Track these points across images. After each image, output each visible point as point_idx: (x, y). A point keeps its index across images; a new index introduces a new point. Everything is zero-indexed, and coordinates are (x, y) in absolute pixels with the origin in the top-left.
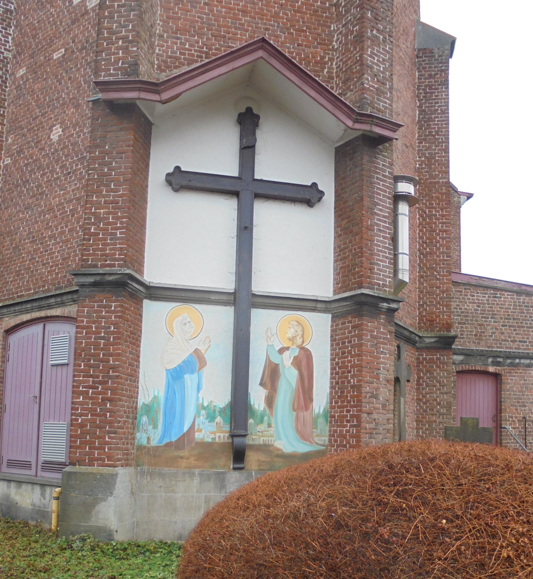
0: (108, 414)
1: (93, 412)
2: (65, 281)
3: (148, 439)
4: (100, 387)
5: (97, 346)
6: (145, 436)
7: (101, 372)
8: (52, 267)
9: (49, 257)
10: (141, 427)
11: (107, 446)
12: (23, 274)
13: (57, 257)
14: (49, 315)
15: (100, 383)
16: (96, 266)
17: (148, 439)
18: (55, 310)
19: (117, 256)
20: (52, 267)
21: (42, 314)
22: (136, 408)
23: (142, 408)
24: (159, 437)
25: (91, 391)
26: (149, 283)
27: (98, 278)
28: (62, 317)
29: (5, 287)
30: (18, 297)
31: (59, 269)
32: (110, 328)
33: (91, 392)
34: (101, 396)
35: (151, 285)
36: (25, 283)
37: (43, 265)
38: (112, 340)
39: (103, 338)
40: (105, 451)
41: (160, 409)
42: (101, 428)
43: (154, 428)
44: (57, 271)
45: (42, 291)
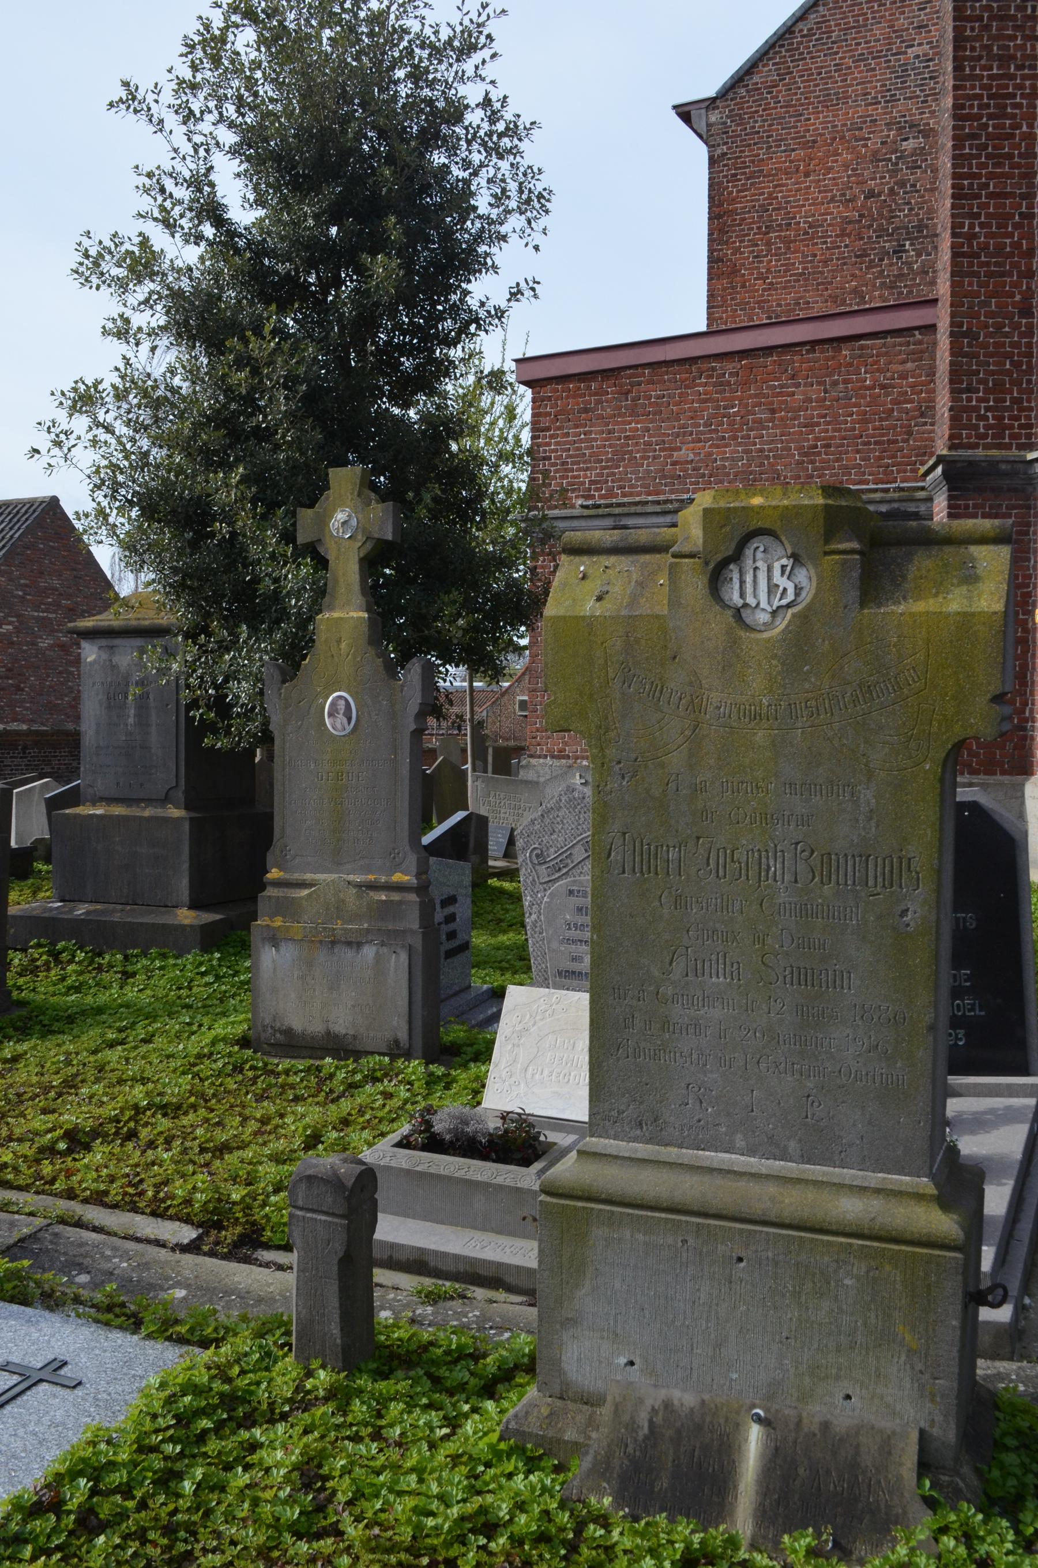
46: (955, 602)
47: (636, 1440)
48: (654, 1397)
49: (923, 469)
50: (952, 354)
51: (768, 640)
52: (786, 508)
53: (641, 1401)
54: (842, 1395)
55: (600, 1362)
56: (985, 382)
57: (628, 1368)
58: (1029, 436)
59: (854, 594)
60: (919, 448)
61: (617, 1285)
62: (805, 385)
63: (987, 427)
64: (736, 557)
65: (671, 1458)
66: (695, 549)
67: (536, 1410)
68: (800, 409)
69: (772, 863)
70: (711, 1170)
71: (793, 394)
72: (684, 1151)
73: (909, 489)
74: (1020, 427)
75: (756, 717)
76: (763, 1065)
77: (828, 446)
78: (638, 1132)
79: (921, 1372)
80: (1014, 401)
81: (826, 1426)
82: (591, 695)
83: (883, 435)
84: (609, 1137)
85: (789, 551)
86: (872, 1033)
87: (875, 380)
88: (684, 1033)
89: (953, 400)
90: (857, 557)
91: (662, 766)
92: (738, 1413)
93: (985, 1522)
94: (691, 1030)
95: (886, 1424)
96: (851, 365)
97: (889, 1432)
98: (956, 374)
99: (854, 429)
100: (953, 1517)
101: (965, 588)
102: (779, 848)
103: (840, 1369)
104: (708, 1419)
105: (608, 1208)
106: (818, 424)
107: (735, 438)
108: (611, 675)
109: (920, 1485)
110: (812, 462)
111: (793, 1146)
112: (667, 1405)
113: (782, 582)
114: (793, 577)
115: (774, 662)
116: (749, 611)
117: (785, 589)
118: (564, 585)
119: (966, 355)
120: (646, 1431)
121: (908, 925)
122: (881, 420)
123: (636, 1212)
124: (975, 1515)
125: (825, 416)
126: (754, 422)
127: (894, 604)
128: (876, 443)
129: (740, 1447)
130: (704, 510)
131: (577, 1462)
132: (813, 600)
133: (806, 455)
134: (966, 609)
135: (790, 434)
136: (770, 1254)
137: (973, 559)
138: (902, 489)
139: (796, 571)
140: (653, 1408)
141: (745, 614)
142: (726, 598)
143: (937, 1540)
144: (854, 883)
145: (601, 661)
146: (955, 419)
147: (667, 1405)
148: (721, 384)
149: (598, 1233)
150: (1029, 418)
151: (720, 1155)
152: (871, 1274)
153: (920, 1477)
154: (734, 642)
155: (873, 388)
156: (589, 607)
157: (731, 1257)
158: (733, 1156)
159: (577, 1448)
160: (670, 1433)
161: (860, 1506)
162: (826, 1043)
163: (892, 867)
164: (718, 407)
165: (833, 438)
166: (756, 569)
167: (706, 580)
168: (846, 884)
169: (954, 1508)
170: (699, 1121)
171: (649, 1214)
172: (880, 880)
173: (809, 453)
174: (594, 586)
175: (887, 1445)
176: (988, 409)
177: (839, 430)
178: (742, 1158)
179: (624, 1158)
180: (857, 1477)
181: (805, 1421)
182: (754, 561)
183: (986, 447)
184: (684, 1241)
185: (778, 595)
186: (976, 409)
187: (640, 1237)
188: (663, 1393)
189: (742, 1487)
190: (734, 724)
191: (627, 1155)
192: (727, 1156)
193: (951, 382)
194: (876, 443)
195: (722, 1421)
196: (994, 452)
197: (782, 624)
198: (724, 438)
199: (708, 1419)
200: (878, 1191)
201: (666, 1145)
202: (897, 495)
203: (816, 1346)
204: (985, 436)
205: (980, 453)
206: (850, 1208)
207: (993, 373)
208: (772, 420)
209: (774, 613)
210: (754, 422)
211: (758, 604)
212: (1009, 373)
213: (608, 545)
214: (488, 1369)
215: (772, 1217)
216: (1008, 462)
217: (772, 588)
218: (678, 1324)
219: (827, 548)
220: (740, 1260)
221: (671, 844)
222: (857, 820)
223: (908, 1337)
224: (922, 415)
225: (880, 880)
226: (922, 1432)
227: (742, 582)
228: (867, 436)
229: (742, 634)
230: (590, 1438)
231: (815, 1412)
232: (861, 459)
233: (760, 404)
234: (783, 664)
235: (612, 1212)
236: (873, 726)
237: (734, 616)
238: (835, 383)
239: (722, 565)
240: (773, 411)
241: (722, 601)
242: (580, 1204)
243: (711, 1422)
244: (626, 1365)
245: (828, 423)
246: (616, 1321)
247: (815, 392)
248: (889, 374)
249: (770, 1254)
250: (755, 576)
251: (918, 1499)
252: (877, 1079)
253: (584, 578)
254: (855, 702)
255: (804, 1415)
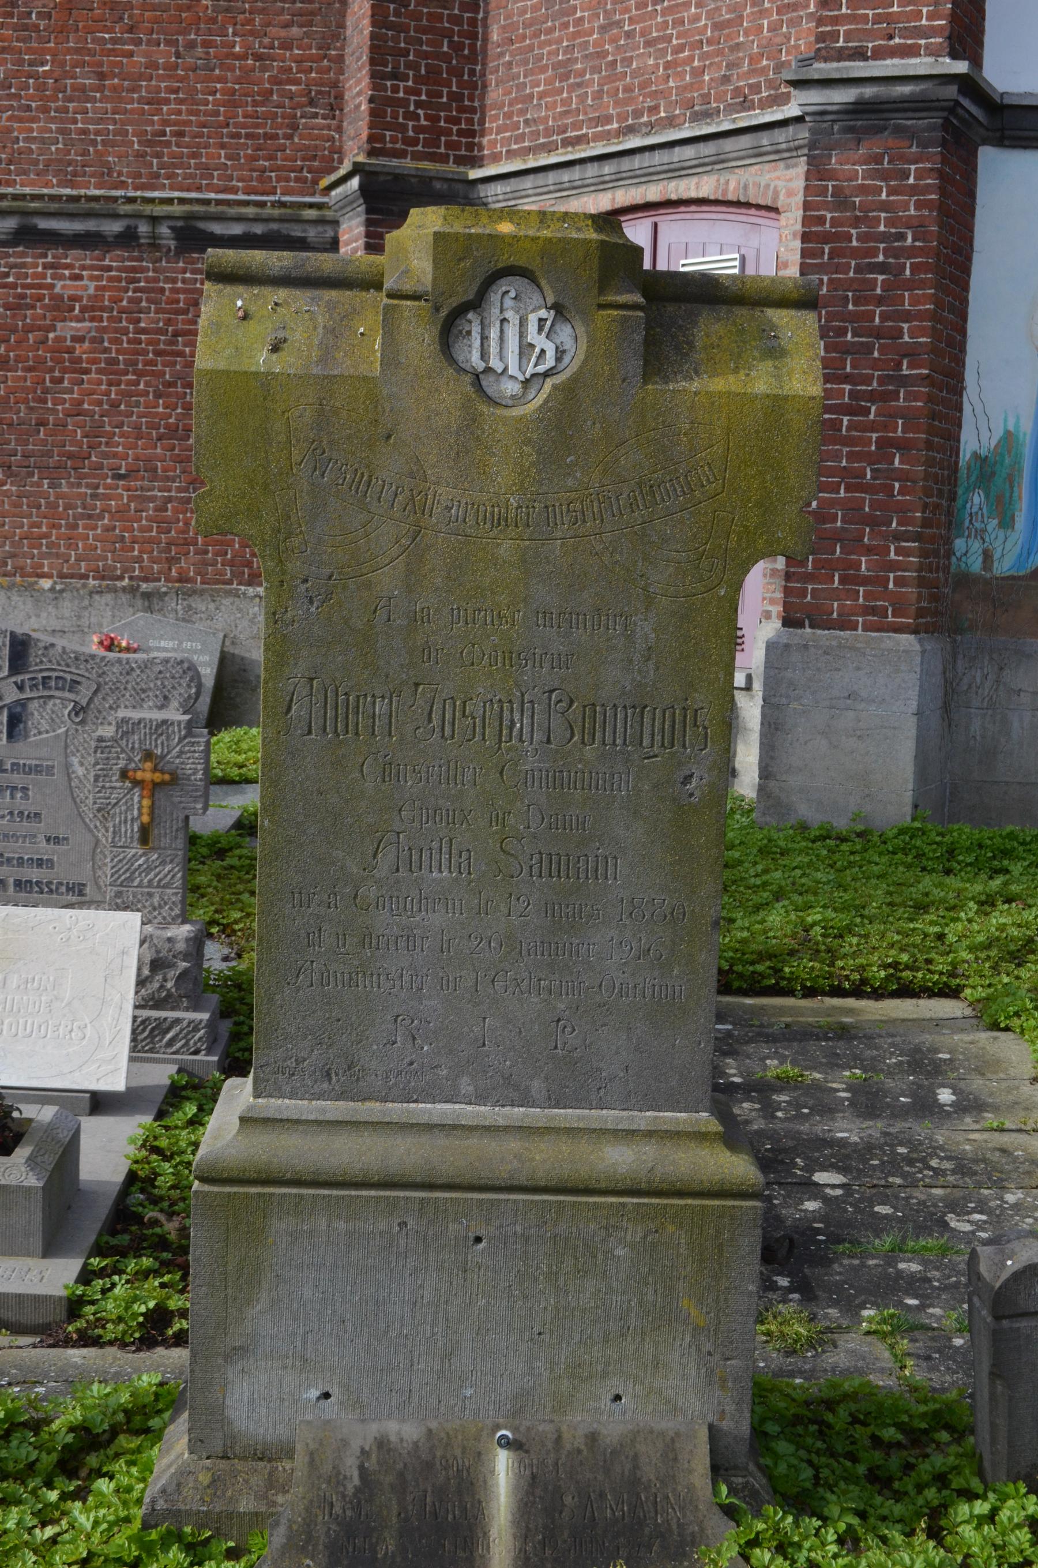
0: (897, 485)
1: (854, 482)
2: (726, 92)
3: (987, 556)
4: (873, 409)
5: (863, 292)
6: (976, 546)
7: (875, 365)
8: (680, 49)
9: (670, 19)
10: (967, 523)
11: (892, 575)
12: (582, 73)
13: (697, 18)
14: (674, 197)
15: (873, 397)
16: (859, 54)
17: (987, 556)
18: (694, 180)
19: (924, 22)
20: (680, 49)
21: (653, 193)
22: (955, 468)
23: (968, 469)
24: (1017, 549)
25: (846, 420)
26: (1002, 94)
27: (869, 91)
28: (716, 202)
29: (523, 112)
30: (568, 143)
31: (703, 57)
32: (902, 237)
33: (845, 423)
34: (874, 435)
35: (1007, 101)
36: (589, 102)
37: (648, 44)
38: (908, 272)
39: (882, 268)
40: (886, 587)
41: (1020, 471)
42: (872, 522)
43: (1002, 525)
44: (696, 63)
45: (645, 124)
46: (761, 381)
47: (344, 1496)
48: (362, 1435)
49: (325, 182)
50: (374, 23)
51: (521, 418)
52: (549, 240)
53: (345, 1443)
54: (610, 1396)
55: (282, 1400)
56: (414, 66)
57: (322, 1402)
58: (470, 147)
59: (635, 365)
60: (307, 148)
61: (308, 1293)
62: (149, 42)
63: (418, 129)
64: (477, 303)
65: (395, 1512)
66: (420, 289)
67: (191, 1478)
68: (141, 77)
69: (517, 717)
70: (429, 1127)
71: (130, 54)
72: (390, 1105)
73: (293, 205)
74: (461, 133)
75: (500, 522)
76: (499, 985)
77: (180, 134)
78: (325, 1085)
79: (710, 1354)
80: (454, 97)
81: (593, 1438)
82: (266, 486)
83: (257, 126)
84: (282, 1096)
85: (551, 300)
86: (643, 935)
87: (248, 47)
88: (392, 947)
89: (375, 87)
90: (641, 314)
91: (368, 585)
92: (478, 1439)
93: (796, 1523)
94: (402, 944)
95: (667, 1425)
96: (213, 20)
97: (671, 1433)
98: (378, 53)
99: (217, 113)
100: (761, 1526)
101: (770, 363)
102: (526, 698)
103: (607, 1364)
104: (439, 1454)
105: (294, 1191)
106: (167, 101)
107: (46, 110)
108: (296, 457)
109: (716, 1493)
110: (159, 155)
111: (537, 1086)
112: (382, 1443)
113: (540, 341)
114: (554, 336)
115: (527, 449)
116: (492, 378)
117: (543, 351)
118: (217, 326)
119: (391, 26)
120: (356, 1481)
121: (691, 795)
122: (255, 103)
123: (335, 1192)
124: (783, 1519)
125: (176, 91)
126: (74, 89)
127: (685, 379)
128: (248, 136)
129: (485, 1482)
130: (435, 234)
131: (258, 1540)
132: (581, 368)
133: (149, 143)
134: (775, 391)
135: (125, 112)
136: (519, 1229)
137: (774, 327)
138: (283, 205)
139: (557, 327)
140: (363, 1451)
141: (486, 381)
142: (461, 359)
143: (746, 1558)
144: (625, 743)
145: (282, 438)
146: (376, 115)
147: (382, 1443)
148: (25, 28)
149: (280, 1226)
150: (470, 121)
151: (438, 1106)
152: (649, 1239)
153: (715, 1483)
154: (473, 420)
155: (243, 57)
156: (261, 360)
157: (466, 1237)
158: (457, 1106)
159: (257, 1520)
160: (389, 1479)
161: (647, 1531)
162: (583, 951)
163: (674, 722)
164: (20, 62)
165: (189, 123)
166: (504, 321)
167: (435, 331)
168: (614, 743)
169: (758, 1514)
170: (411, 1063)
171: (353, 1193)
172: (658, 738)
173: (154, 141)
174: (261, 331)
175: (671, 1450)
176: (419, 104)
177: (197, 113)
178: (469, 1108)
179: (307, 1122)
180: (639, 1497)
181: (566, 1436)
182: (502, 311)
183: (417, 157)
184: (403, 1224)
185: (533, 359)
186: (405, 103)
187: (341, 1225)
188: (374, 1429)
189: (494, 1533)
190: (469, 531)
191: (312, 1117)
192: (449, 1106)
193: (373, 62)
194: (248, 136)
195: (458, 1452)
196: (425, 165)
197: (538, 398)
198: (29, 108)
199: (439, 1454)
200: (650, 1134)
201: (365, 1100)
202: (276, 212)
203: (577, 1339)
204: (415, 142)
205: (408, 164)
206: (620, 1159)
207: (426, 55)
208: (101, 89)
209: (526, 383)
210: (74, 89)
211: (506, 369)
212: (446, 58)
213: (276, 272)
214: (59, 1438)
215: (541, 1178)
216: (446, 180)
217: (525, 348)
218: (392, 1334)
219: (603, 299)
220: (478, 1240)
221: (378, 693)
222: (631, 661)
223: (694, 1312)
224: (311, 103)
225: (658, 738)
226: (711, 1427)
227: (484, 338)
228: (237, 125)
229: (485, 409)
230: (274, 1504)
231: (577, 1423)
232: (227, 158)
233: (82, 64)
234: (539, 452)
235: (301, 1197)
236: (655, 538)
237: (473, 385)
238: (191, 45)
239: (460, 311)
240: (102, 76)
241: (456, 362)
242: (253, 1190)
243: (444, 1457)
244: (318, 1399)
245: (181, 102)
246: (305, 1342)
247: (163, 54)
248: (266, 40)
249: (519, 1229)
250: (502, 331)
251: (716, 1509)
252: (648, 993)
253: (245, 318)
254: (632, 506)
255: (564, 1428)
